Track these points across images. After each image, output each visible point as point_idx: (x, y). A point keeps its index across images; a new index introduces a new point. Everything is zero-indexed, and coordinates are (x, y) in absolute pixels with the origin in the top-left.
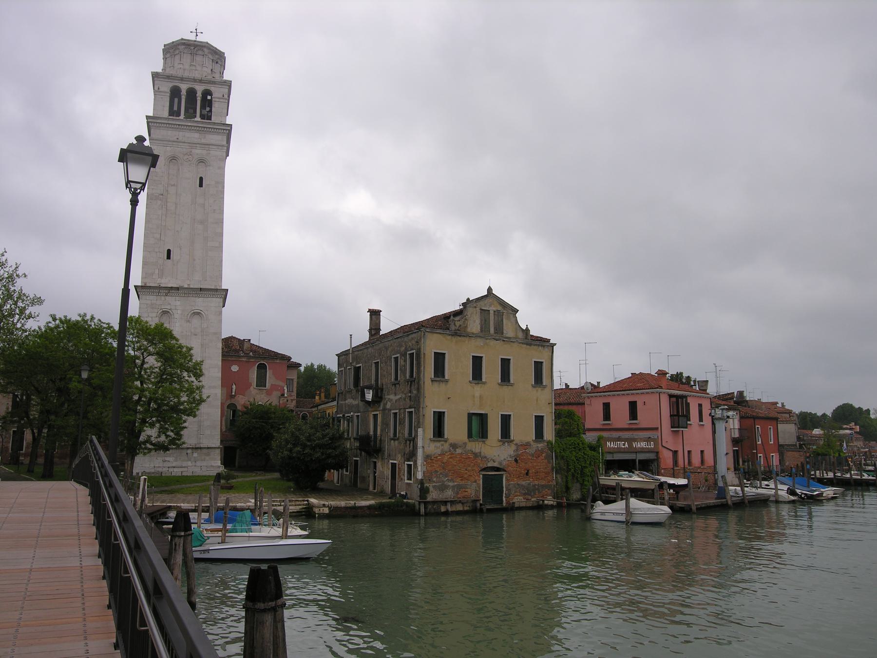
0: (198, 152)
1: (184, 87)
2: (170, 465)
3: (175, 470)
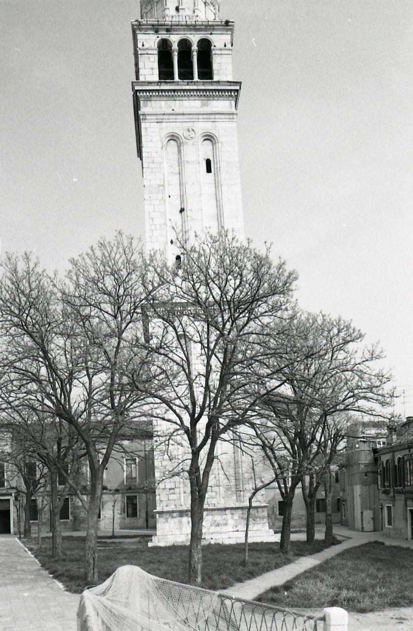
0: (202, 127)
1: (175, 39)
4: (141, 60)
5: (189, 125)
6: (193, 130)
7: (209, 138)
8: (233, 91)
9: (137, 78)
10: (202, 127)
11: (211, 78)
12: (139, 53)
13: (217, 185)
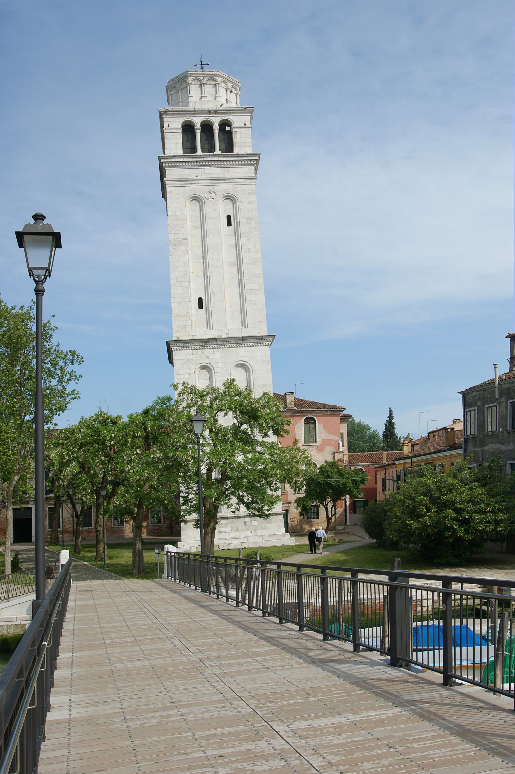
0: (223, 189)
1: (197, 121)
2: (227, 536)
3: (234, 541)
4: (167, 136)
5: (211, 188)
6: (214, 192)
7: (229, 198)
8: (253, 159)
9: (164, 153)
10: (223, 189)
11: (232, 150)
12: (165, 131)
13: (237, 235)
